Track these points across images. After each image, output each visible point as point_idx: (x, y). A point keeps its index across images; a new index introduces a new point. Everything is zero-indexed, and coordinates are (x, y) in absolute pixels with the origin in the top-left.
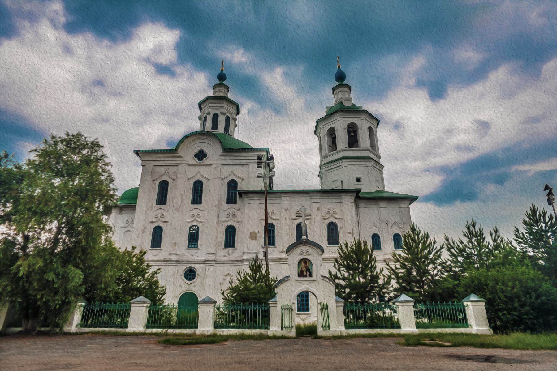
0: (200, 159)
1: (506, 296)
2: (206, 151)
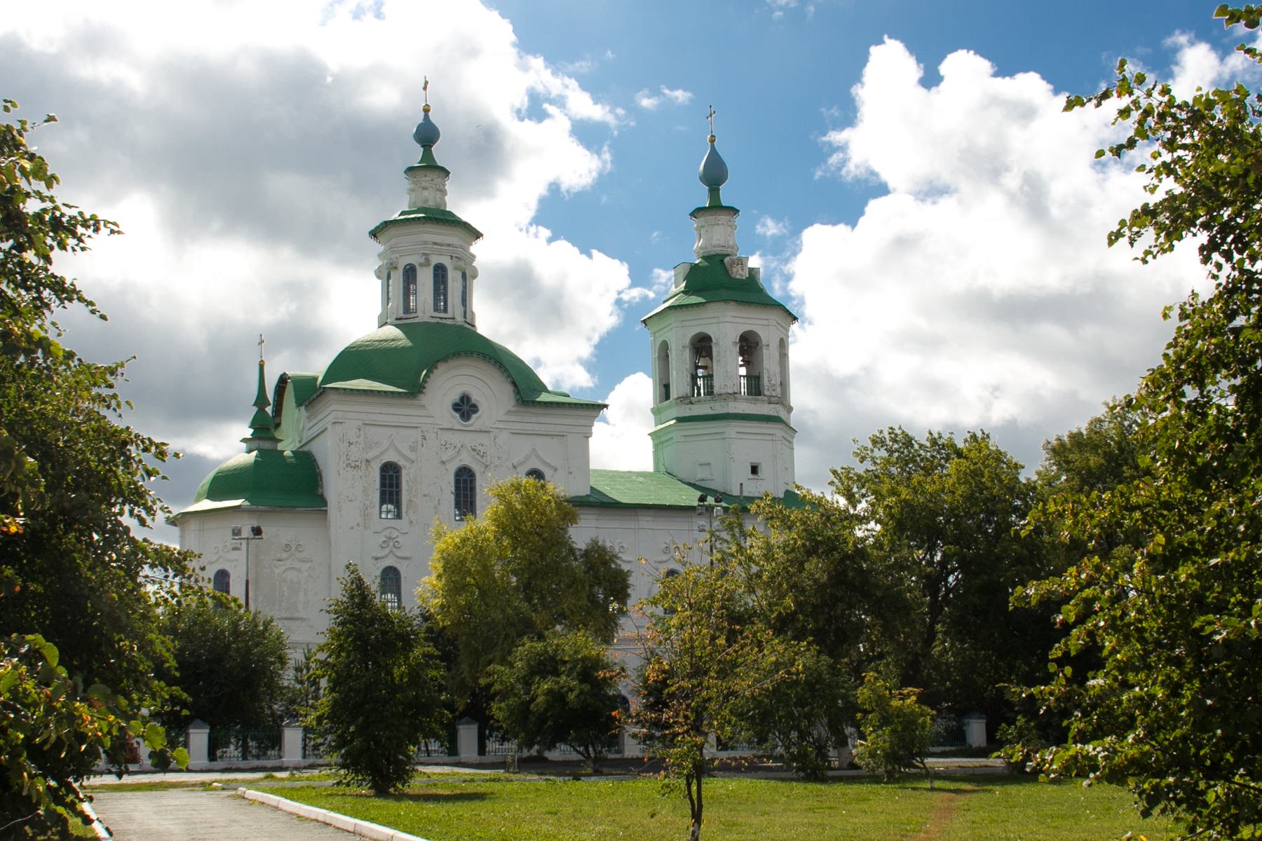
1: (166, 570)
2: (476, 397)
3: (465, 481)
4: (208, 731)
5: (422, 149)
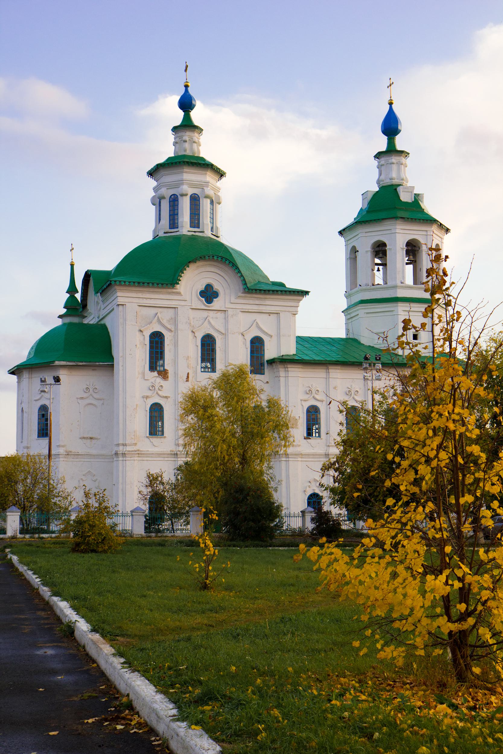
0: (209, 300)
2: (217, 286)
3: (157, 343)
4: (19, 514)
5: (183, 113)
